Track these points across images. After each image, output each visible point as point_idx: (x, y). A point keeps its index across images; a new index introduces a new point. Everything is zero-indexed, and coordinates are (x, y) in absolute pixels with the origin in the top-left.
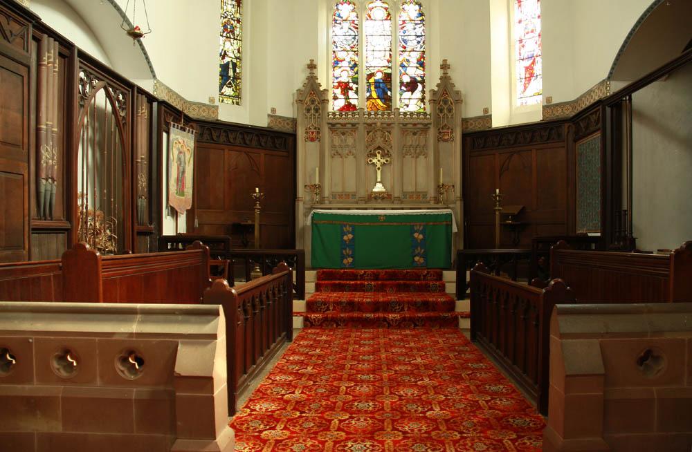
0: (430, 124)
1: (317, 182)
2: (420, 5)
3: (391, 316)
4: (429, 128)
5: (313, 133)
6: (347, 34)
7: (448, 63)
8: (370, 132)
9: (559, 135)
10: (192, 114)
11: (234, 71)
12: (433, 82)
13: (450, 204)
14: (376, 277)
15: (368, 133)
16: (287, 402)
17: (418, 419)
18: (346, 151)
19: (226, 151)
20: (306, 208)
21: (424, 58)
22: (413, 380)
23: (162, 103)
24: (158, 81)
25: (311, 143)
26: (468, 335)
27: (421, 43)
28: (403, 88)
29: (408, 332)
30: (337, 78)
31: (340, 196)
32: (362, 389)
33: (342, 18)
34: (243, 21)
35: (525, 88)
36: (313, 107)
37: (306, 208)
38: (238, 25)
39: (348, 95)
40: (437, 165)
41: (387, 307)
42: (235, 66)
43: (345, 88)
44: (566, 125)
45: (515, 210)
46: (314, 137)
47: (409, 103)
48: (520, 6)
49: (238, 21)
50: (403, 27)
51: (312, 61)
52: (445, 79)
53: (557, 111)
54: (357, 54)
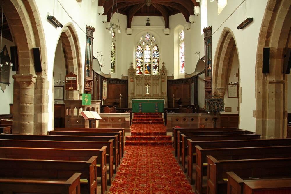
2: (158, 47)
3: (150, 122)
10: (106, 77)
12: (161, 68)
14: (147, 114)
15: (145, 80)
16: (118, 184)
17: (159, 178)
19: (113, 85)
22: (158, 167)
23: (102, 76)
28: (154, 68)
29: (157, 147)
31: (138, 95)
32: (142, 179)
36: (132, 73)
40: (161, 88)
41: (149, 120)
42: (113, 63)
43: (139, 68)
45: (179, 99)
46: (132, 81)
47: (155, 72)
49: (114, 52)
51: (132, 62)
52: (163, 67)
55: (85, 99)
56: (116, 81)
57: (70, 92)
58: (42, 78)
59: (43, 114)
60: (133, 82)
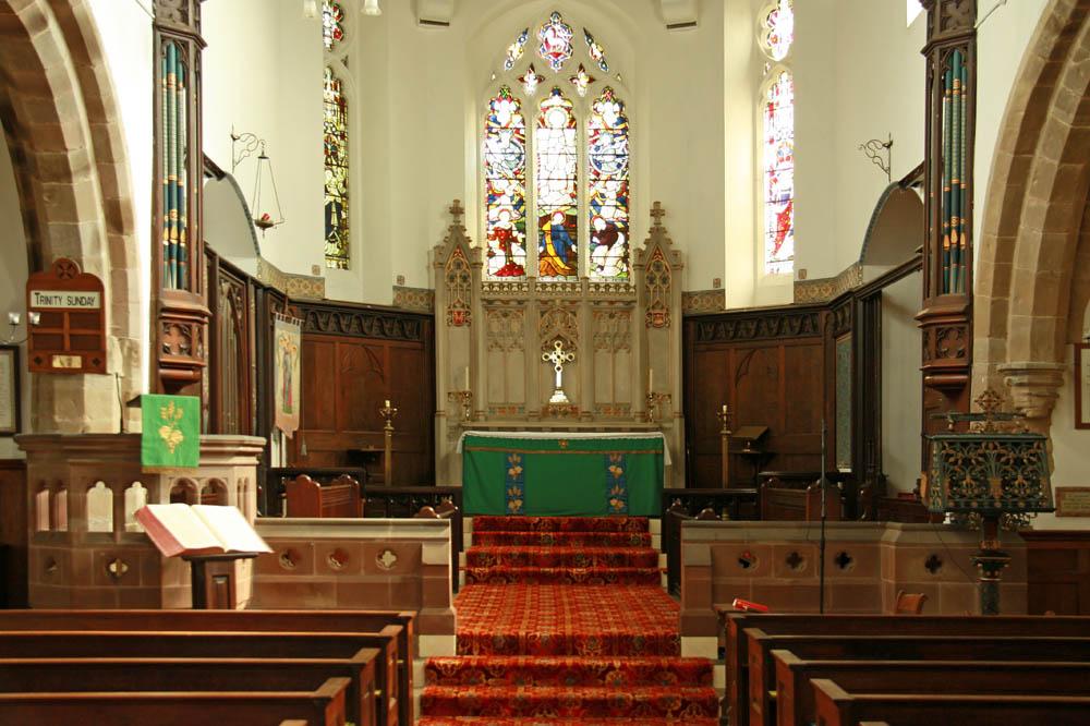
0: (635, 301)
1: (467, 389)
2: (622, 105)
4: (633, 308)
5: (459, 313)
6: (508, 151)
7: (662, 207)
8: (546, 312)
9: (815, 327)
10: (293, 294)
12: (640, 237)
13: (666, 422)
14: (556, 526)
15: (542, 314)
18: (510, 341)
20: (451, 428)
21: (627, 191)
24: (262, 259)
25: (457, 329)
26: (666, 591)
27: (623, 168)
28: (595, 239)
30: (493, 223)
31: (502, 409)
33: (499, 124)
34: (351, 136)
35: (778, 246)
36: (458, 273)
37: (451, 428)
38: (342, 143)
39: (511, 251)
40: (645, 365)
41: (570, 560)
42: (339, 207)
43: (506, 238)
44: (825, 313)
45: (754, 432)
46: (462, 319)
47: (604, 265)
48: (772, 116)
49: (343, 136)
50: (596, 141)
52: (657, 231)
53: (813, 291)
54: (524, 184)
55: (165, 432)
57: (59, 384)
60: (465, 327)
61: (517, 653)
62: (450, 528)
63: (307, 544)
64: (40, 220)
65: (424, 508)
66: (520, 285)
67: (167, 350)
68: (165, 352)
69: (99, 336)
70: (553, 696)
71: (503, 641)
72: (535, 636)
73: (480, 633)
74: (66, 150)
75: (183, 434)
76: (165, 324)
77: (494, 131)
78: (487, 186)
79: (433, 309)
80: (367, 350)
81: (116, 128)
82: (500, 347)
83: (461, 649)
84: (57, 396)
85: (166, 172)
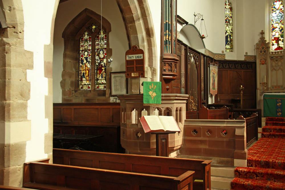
1: (265, 82)
10: (216, 58)
11: (230, 38)
19: (229, 71)
20: (261, 92)
23: (208, 57)
24: (206, 49)
30: (274, 36)
31: (276, 87)
33: (276, 8)
36: (263, 50)
38: (231, 19)
39: (279, 43)
42: (230, 36)
43: (277, 40)
49: (231, 17)
55: (150, 93)
56: (240, 64)
57: (134, 81)
58: (4, 42)
59: (7, 123)
60: (265, 65)
61: (269, 167)
62: (245, 123)
63: (200, 128)
64: (129, 35)
65: (240, 116)
66: (281, 52)
67: (165, 70)
68: (164, 71)
69: (143, 67)
70: (281, 188)
71: (264, 163)
72: (276, 162)
73: (256, 159)
74: (133, 14)
75: (156, 94)
76: (164, 63)
77: (274, 11)
78: (272, 26)
79: (256, 61)
80: (237, 72)
81: (146, 6)
82: (275, 70)
83: (249, 165)
84: (133, 84)
85: (165, 20)
